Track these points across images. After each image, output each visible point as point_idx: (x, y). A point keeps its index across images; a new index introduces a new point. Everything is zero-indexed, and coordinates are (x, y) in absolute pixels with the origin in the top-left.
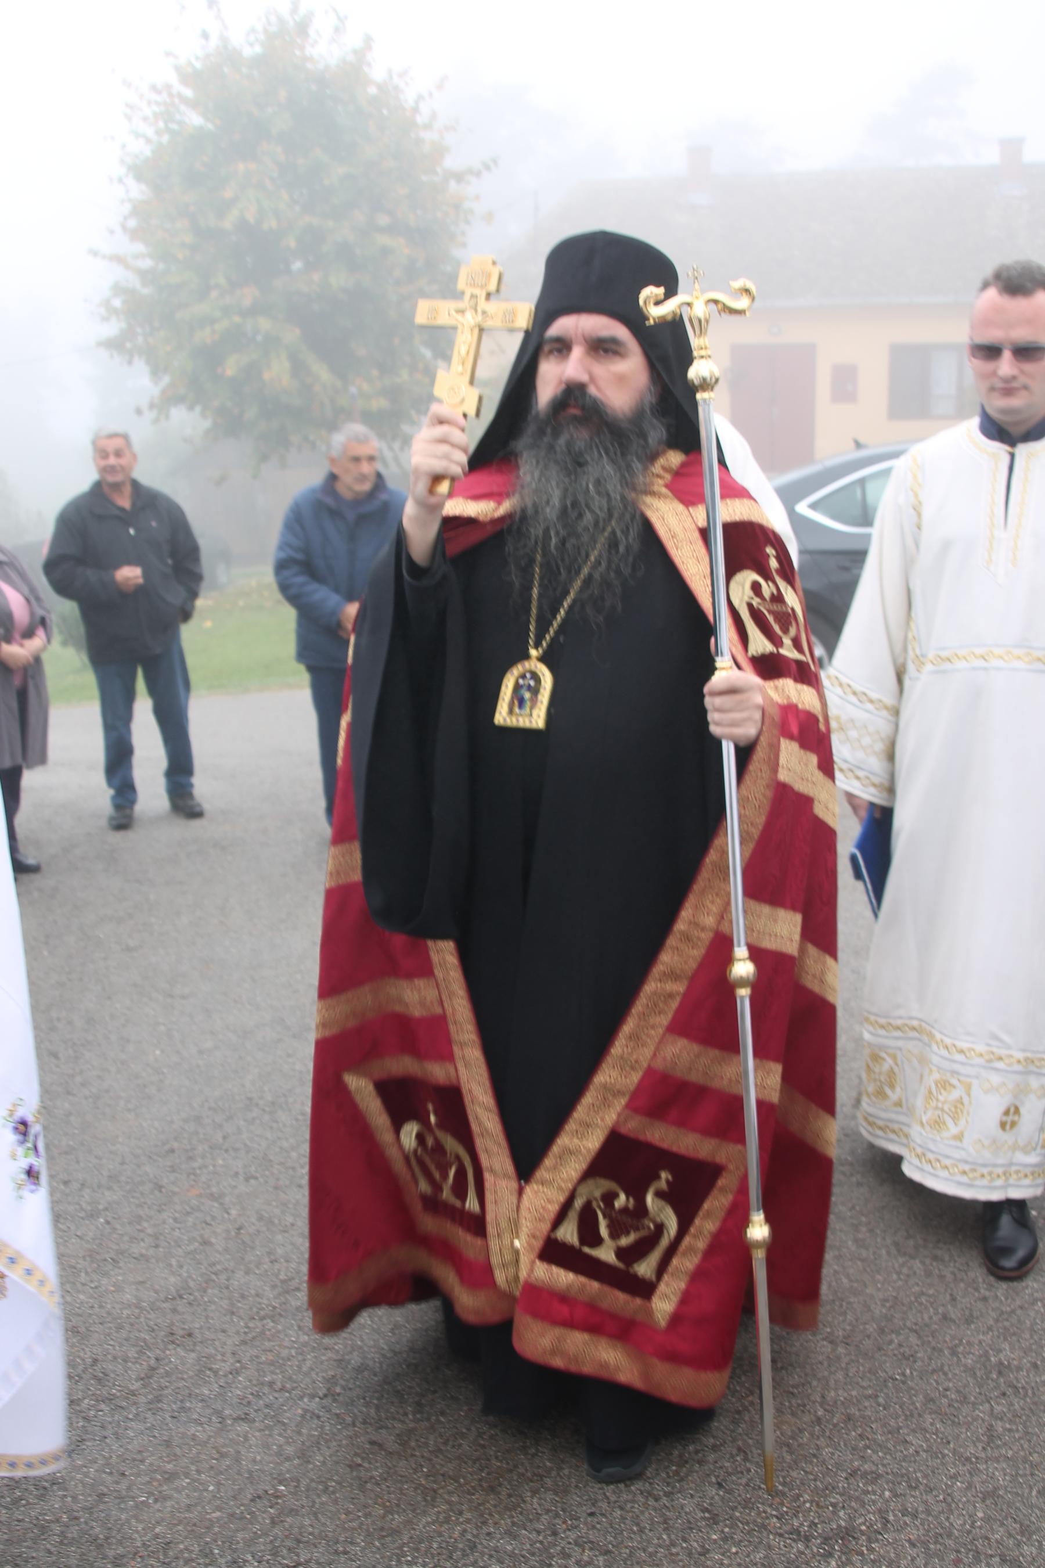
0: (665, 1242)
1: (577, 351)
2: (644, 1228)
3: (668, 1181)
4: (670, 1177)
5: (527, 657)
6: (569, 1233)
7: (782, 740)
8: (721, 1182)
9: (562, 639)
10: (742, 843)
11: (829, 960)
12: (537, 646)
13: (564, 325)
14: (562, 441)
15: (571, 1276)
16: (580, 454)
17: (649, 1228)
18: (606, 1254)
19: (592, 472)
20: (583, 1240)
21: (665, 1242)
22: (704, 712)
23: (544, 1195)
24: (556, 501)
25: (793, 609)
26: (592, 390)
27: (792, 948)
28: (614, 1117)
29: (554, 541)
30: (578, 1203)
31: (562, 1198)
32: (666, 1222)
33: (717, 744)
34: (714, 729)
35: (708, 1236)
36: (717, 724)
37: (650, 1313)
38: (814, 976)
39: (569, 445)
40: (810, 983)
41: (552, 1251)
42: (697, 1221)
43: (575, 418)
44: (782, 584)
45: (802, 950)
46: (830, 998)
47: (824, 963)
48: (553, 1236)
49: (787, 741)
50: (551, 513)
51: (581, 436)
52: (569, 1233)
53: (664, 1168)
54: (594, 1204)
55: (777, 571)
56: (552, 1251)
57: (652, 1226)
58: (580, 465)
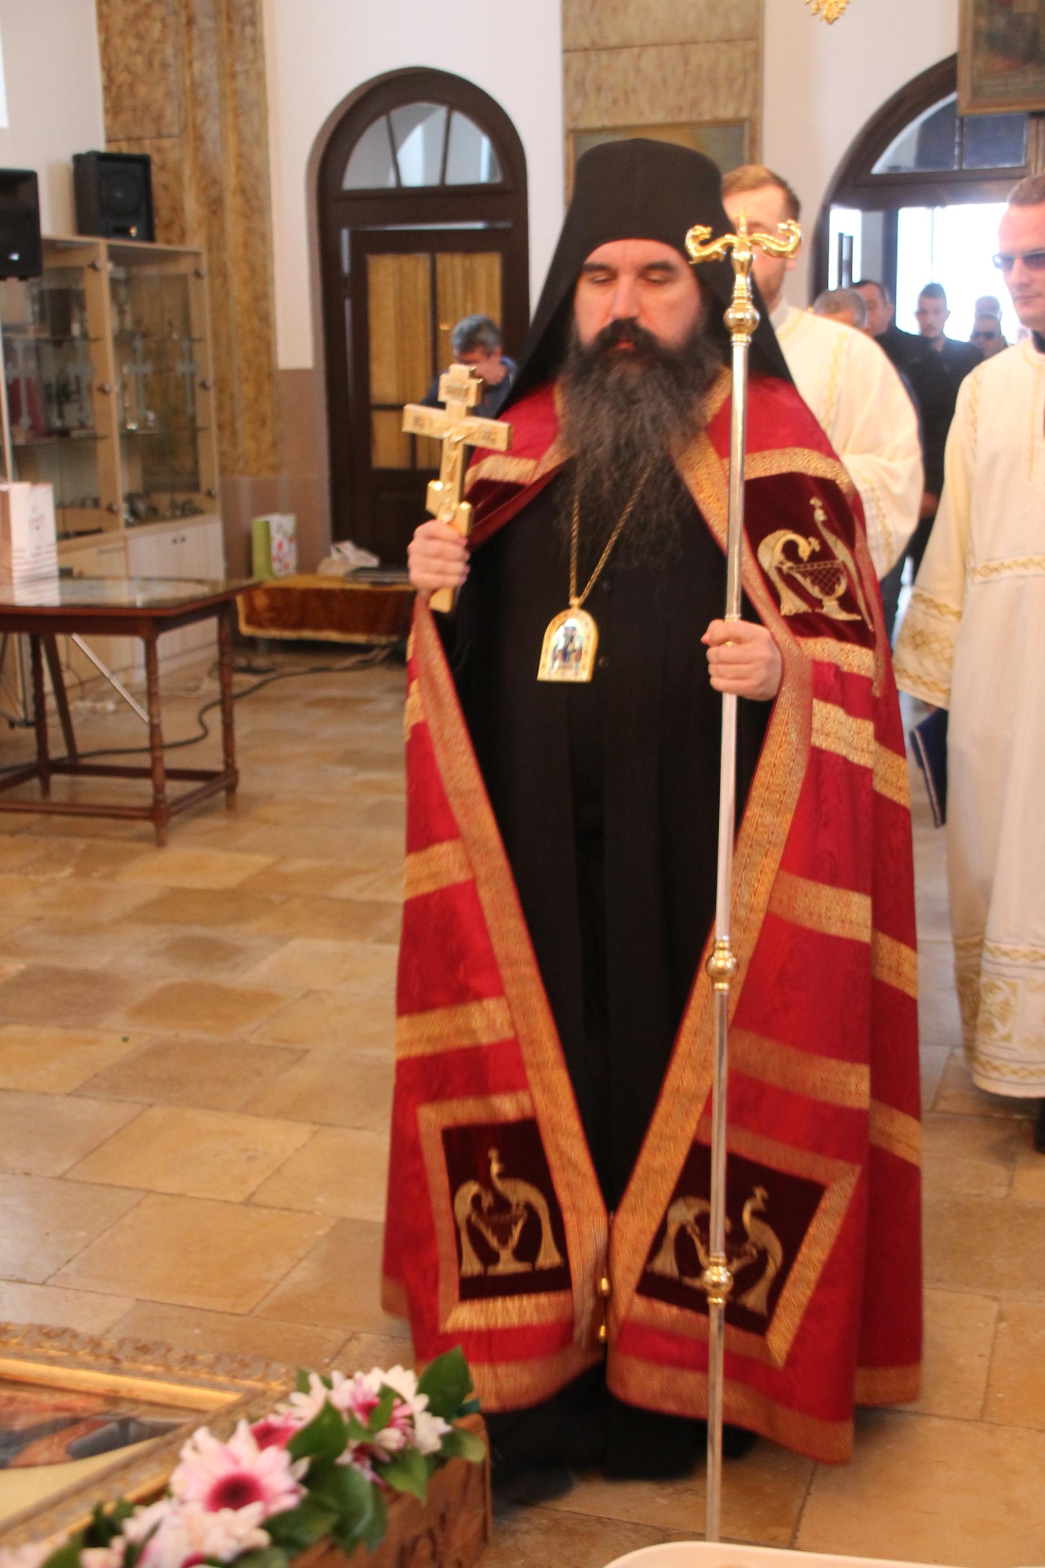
0: (771, 1270)
1: (625, 281)
2: (746, 1254)
3: (763, 1200)
4: (765, 1195)
5: (568, 607)
6: (667, 1264)
7: (815, 701)
8: (824, 1204)
9: (605, 585)
10: (138, 701)
11: (905, 950)
12: (579, 594)
13: (607, 253)
14: (612, 378)
15: (675, 1311)
16: (633, 391)
17: (752, 1254)
18: (507, 1265)
19: (646, 410)
20: (682, 1271)
21: (771, 1270)
22: (706, 663)
23: (637, 1223)
24: (608, 441)
25: (844, 563)
26: (643, 323)
27: (864, 934)
28: (694, 1126)
29: (607, 484)
30: (672, 1231)
31: (654, 1227)
32: (769, 1248)
33: (716, 698)
34: (716, 682)
35: (819, 1265)
36: (721, 676)
37: (766, 1350)
38: (890, 968)
39: (621, 382)
40: (887, 976)
41: (651, 1285)
42: (804, 1249)
43: (625, 354)
44: (831, 539)
45: (874, 940)
46: (909, 991)
47: (899, 952)
48: (649, 1270)
49: (821, 704)
50: (602, 452)
51: (634, 372)
52: (667, 1264)
53: (757, 1184)
54: (689, 1229)
55: (824, 523)
56: (651, 1285)
57: (754, 1252)
58: (633, 402)
